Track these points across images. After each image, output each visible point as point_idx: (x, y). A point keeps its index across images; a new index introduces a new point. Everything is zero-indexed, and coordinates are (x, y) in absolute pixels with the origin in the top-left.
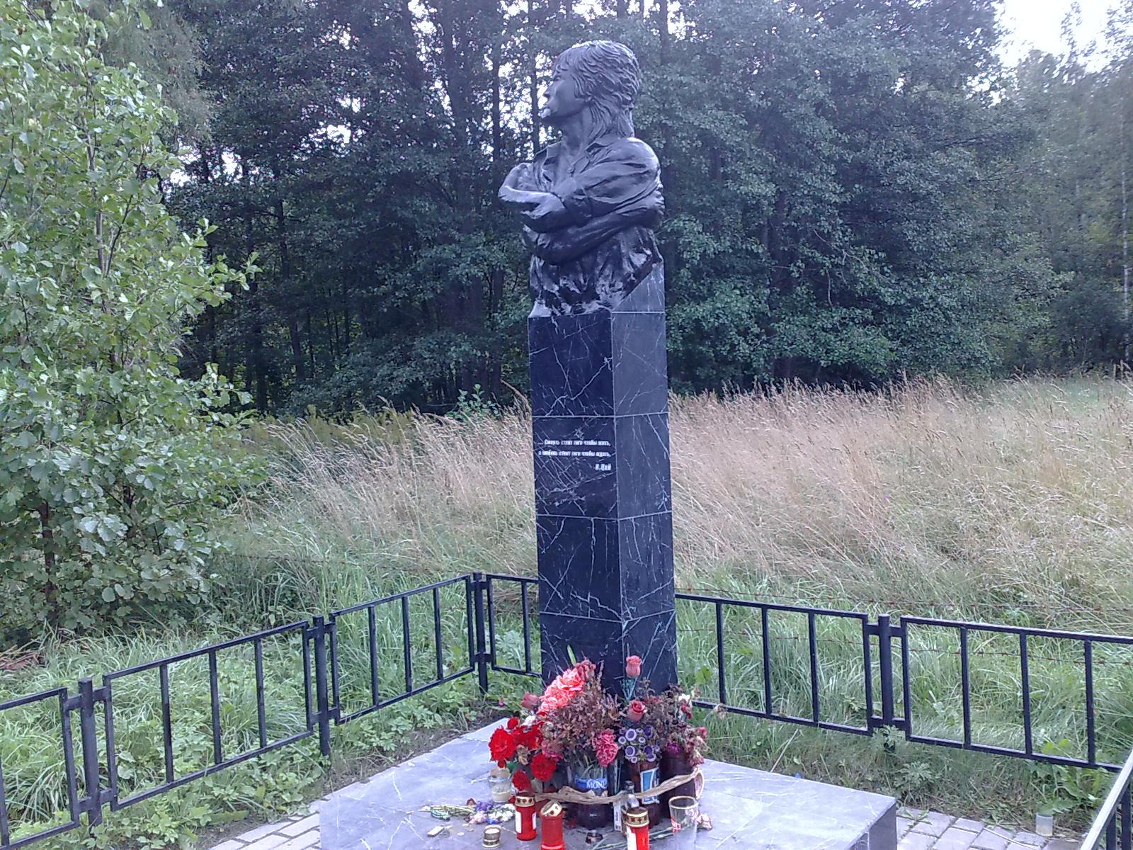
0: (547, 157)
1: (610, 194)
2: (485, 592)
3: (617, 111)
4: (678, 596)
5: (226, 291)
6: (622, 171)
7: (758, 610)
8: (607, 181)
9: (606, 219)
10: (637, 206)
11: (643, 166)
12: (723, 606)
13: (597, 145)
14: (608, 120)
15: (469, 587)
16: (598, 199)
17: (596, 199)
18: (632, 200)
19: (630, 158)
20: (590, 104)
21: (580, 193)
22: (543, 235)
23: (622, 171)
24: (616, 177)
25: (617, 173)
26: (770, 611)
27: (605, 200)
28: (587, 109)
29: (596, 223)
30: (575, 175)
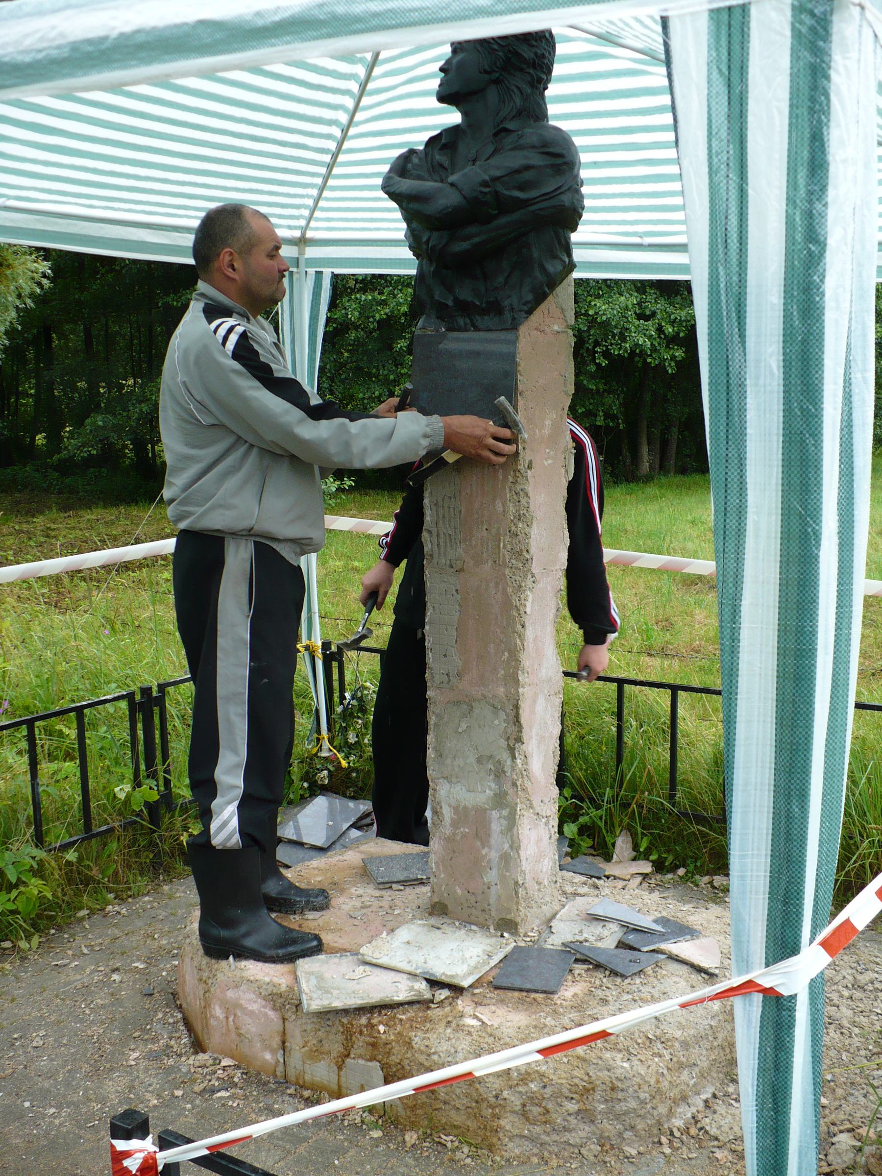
0: (443, 141)
1: (521, 188)
2: (156, 710)
3: (529, 91)
4: (719, 693)
5: (335, 480)
6: (536, 160)
7: (614, 686)
8: (518, 171)
9: (516, 216)
10: (553, 202)
11: (561, 156)
12: (682, 694)
13: (505, 130)
14: (518, 101)
15: (133, 707)
16: (508, 193)
17: (505, 192)
18: (548, 196)
19: (543, 146)
20: (497, 82)
21: (485, 184)
22: (435, 234)
23: (536, 160)
24: (528, 168)
25: (532, 162)
26: (682, 694)
27: (517, 194)
28: (493, 87)
29: (503, 220)
30: (478, 163)
